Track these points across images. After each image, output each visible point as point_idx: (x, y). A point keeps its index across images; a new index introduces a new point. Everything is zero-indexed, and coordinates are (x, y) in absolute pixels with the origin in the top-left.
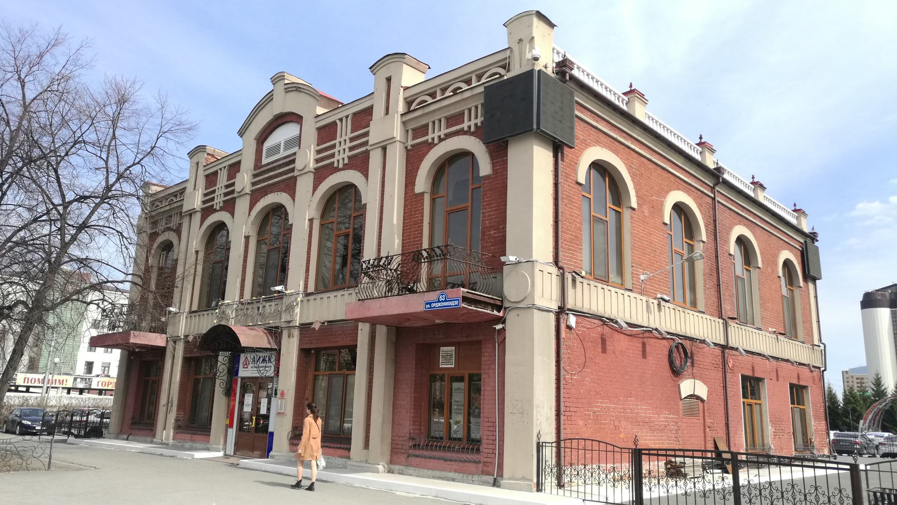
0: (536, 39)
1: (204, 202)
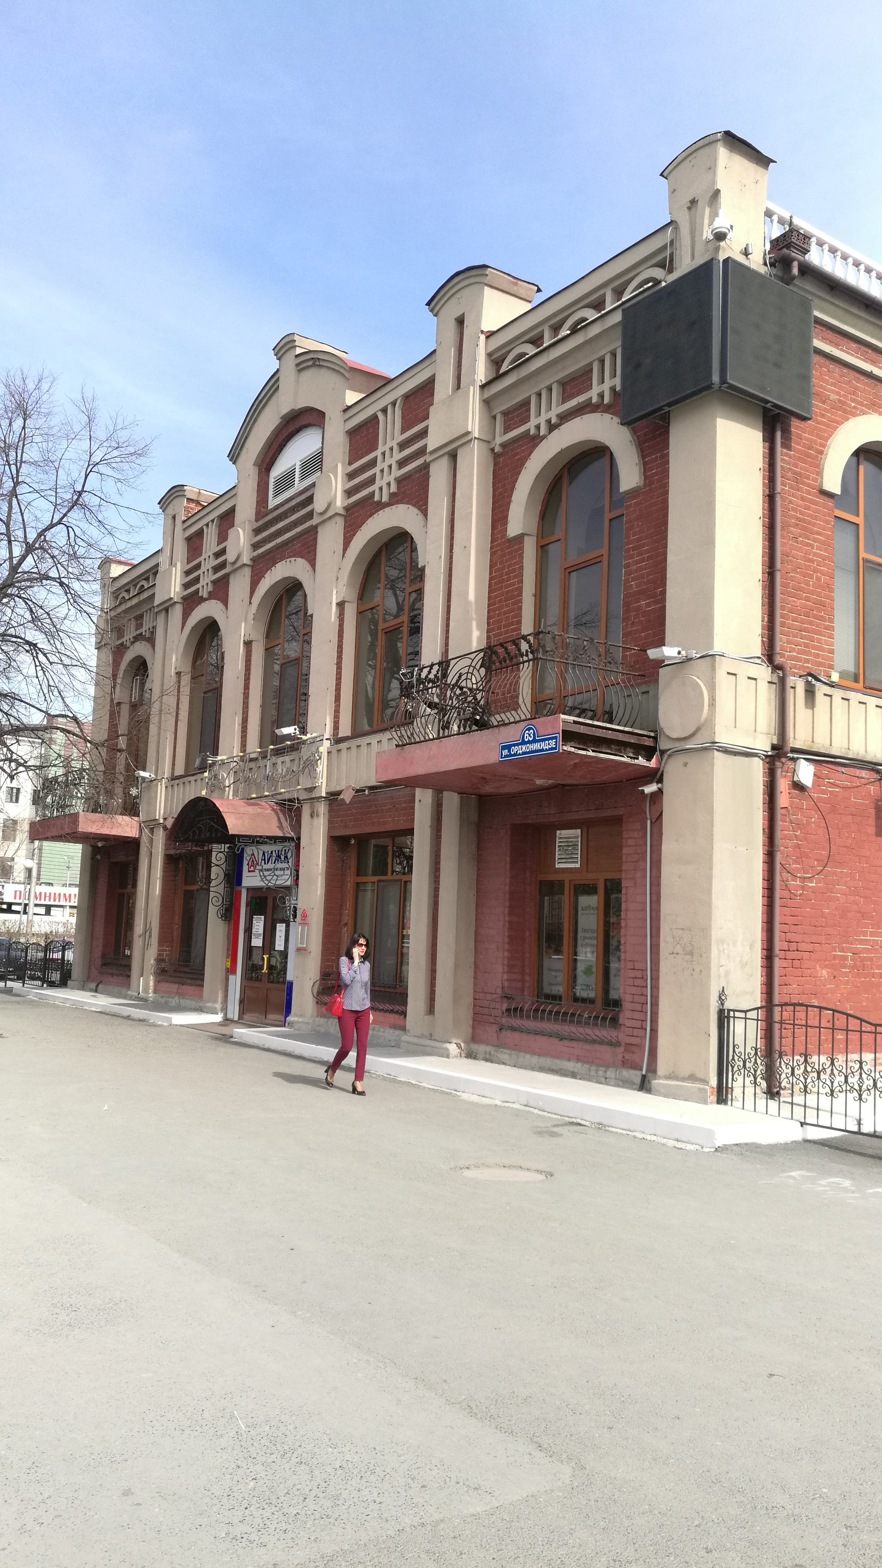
0: (724, 198)
1: (186, 586)
